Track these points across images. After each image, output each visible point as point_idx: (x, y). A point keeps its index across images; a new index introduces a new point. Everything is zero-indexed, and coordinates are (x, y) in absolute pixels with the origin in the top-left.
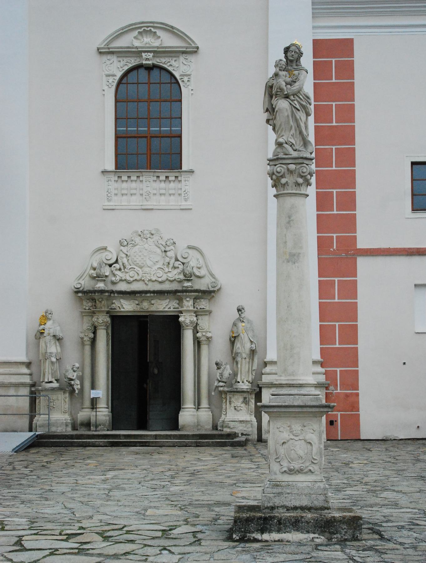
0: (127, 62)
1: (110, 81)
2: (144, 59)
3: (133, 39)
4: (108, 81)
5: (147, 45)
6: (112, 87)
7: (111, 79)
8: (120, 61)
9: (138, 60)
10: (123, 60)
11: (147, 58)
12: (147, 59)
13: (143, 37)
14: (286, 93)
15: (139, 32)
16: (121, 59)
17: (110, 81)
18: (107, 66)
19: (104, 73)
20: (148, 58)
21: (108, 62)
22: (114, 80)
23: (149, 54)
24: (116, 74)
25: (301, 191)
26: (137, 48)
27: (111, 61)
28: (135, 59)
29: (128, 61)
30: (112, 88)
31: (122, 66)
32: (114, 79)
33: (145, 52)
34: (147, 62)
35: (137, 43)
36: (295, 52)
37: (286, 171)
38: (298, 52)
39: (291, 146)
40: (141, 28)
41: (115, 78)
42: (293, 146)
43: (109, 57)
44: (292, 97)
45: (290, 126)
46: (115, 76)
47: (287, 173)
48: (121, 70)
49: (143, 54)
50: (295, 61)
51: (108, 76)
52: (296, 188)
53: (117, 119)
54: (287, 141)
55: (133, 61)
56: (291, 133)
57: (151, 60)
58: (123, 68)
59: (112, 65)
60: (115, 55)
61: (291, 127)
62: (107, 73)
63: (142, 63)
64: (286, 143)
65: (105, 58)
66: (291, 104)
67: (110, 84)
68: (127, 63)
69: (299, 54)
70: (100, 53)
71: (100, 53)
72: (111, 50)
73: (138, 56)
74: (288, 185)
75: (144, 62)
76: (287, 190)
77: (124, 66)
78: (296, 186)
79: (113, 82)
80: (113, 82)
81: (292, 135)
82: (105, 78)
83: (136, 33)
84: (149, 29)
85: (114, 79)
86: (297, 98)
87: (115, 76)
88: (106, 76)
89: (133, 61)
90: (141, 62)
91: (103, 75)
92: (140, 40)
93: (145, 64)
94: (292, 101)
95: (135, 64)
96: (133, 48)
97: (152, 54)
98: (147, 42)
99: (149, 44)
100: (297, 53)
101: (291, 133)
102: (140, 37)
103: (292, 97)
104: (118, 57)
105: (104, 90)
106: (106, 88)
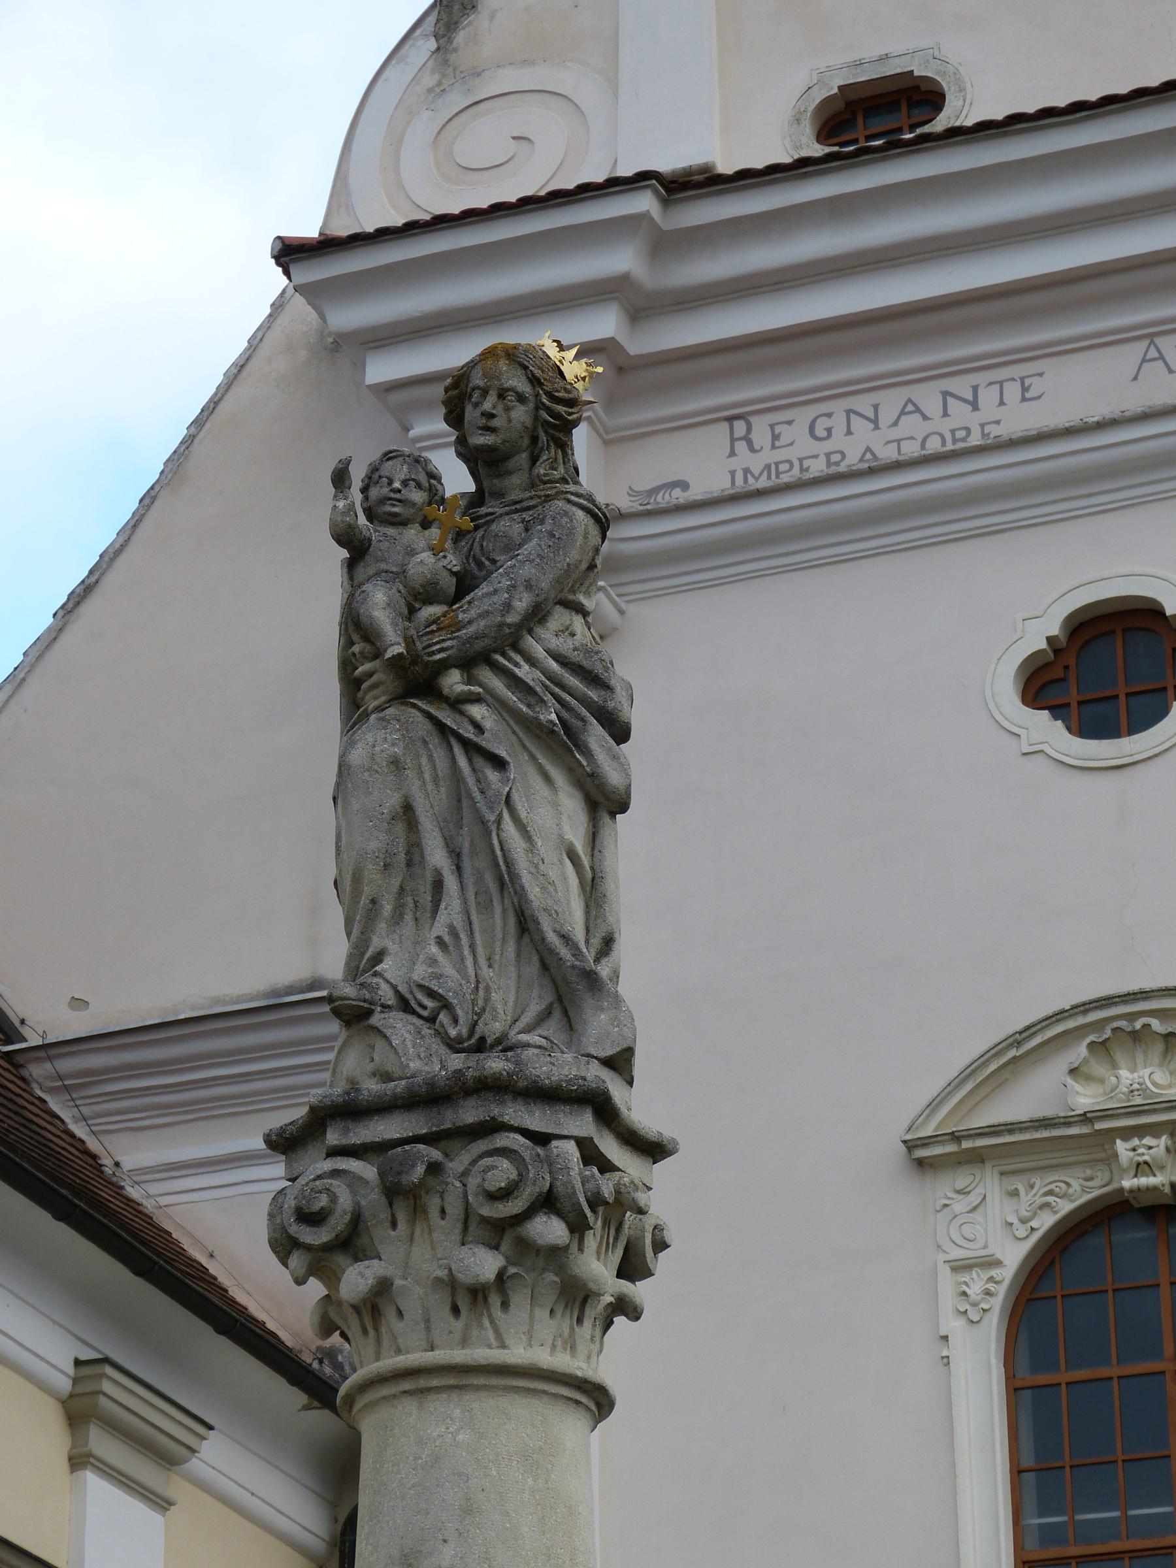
0: (1050, 1193)
1: (974, 1291)
2: (1123, 1171)
3: (1069, 1081)
4: (964, 1294)
5: (1138, 1101)
6: (987, 1316)
7: (976, 1284)
8: (1015, 1194)
9: (1101, 1177)
10: (1032, 1187)
11: (1140, 1159)
12: (1141, 1168)
13: (1114, 1066)
14: (399, 649)
15: (1091, 1045)
16: (1019, 1184)
17: (974, 1291)
18: (958, 1221)
19: (942, 1257)
20: (1147, 1158)
21: (960, 1205)
22: (991, 1286)
23: (1148, 1141)
24: (999, 1255)
25: (503, 1346)
26: (1086, 1118)
27: (974, 1199)
28: (1089, 1172)
29: (1052, 1186)
30: (984, 1323)
31: (1024, 1213)
32: (991, 1279)
33: (1127, 1133)
34: (1144, 1181)
35: (1085, 1098)
36: (501, 396)
37: (372, 1198)
38: (524, 387)
39: (431, 1020)
40: (1099, 1025)
41: (995, 1273)
42: (443, 1017)
43: (962, 1179)
44: (454, 682)
45: (429, 877)
46: (998, 1263)
47: (385, 1215)
48: (1021, 1232)
49: (1121, 1146)
50: (523, 458)
51: (960, 1267)
52: (458, 1325)
53: (1019, 1472)
54: (403, 989)
55: (1076, 1185)
56: (440, 928)
57: (1162, 1168)
58: (1034, 1224)
59: (977, 1216)
60: (988, 1166)
61: (438, 885)
62: (956, 1253)
63: (1121, 1190)
64: (405, 1006)
65: (944, 1186)
66: (442, 729)
67: (975, 1305)
68: (1050, 1199)
69: (539, 406)
70: (921, 1163)
71: (921, 1163)
72: (966, 1144)
73: (1102, 1155)
74: (400, 1314)
75: (1128, 1183)
76: (399, 1351)
77: (1034, 1215)
78: (456, 1310)
79: (988, 1293)
80: (988, 1293)
81: (440, 941)
82: (947, 1281)
83: (1080, 1051)
84: (1138, 1025)
85: (991, 1279)
86: (497, 684)
87: (998, 1263)
88: (954, 1269)
89: (1076, 1185)
90: (1115, 1186)
91: (940, 1264)
92: (1102, 1081)
93: (1131, 1191)
94: (456, 704)
95: (1086, 1198)
96: (1067, 1123)
97: (1164, 1138)
98: (1136, 1086)
99: (1143, 1090)
100: (521, 399)
101: (440, 928)
102: (1098, 1068)
103: (454, 682)
104: (1002, 1174)
105: (945, 1338)
106: (953, 1325)
